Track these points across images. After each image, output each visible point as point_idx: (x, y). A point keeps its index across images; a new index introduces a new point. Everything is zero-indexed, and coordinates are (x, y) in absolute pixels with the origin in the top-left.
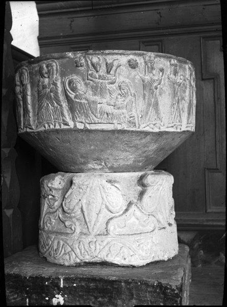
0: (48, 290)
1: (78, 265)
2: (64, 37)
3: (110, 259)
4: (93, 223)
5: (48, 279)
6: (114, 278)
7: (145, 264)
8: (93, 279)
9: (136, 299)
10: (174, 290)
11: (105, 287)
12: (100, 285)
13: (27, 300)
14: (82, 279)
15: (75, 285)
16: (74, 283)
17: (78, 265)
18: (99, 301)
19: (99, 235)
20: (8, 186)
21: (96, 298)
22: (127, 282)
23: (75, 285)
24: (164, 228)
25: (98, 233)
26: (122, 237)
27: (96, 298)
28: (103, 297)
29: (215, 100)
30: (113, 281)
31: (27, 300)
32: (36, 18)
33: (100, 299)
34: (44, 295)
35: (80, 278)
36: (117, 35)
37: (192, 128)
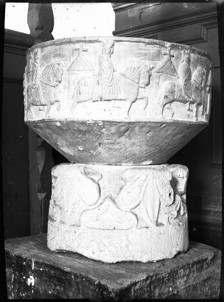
0: (25, 270)
1: (60, 252)
2: (133, 29)
3: (80, 251)
4: (69, 212)
5: (25, 260)
6: (67, 269)
7: (115, 262)
8: (52, 267)
9: (82, 295)
10: (110, 293)
11: (61, 277)
12: (58, 274)
13: (13, 275)
14: (46, 265)
15: (41, 269)
16: (41, 268)
17: (61, 252)
18: (57, 290)
19: (73, 225)
20: (40, 171)
21: (56, 285)
22: (75, 275)
23: (41, 269)
24: (147, 228)
25: (73, 223)
26: (93, 230)
27: (56, 285)
28: (60, 286)
29: (11, 35)
30: (67, 272)
31: (13, 275)
32: (113, 15)
33: (58, 288)
34: (23, 274)
35: (45, 264)
36: (179, 21)
37: (203, 119)
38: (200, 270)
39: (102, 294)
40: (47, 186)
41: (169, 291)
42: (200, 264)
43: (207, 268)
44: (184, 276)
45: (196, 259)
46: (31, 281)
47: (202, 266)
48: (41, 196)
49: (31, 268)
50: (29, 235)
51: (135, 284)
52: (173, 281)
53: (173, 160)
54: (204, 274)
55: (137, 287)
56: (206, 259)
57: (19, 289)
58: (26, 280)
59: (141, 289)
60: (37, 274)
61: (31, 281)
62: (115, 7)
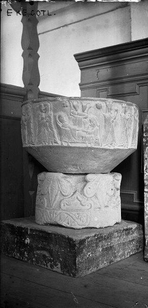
17: (46, 224)
20: (31, 177)
38: (127, 234)
39: (70, 243)
40: (34, 186)
41: (108, 244)
42: (128, 231)
43: (132, 234)
44: (118, 236)
45: (125, 228)
46: (28, 241)
47: (129, 233)
48: (31, 193)
49: (27, 233)
50: (19, 119)
51: (88, 238)
52: (111, 239)
53: (115, 170)
54: (130, 237)
55: (89, 240)
56: (132, 228)
57: (20, 247)
58: (24, 241)
59: (92, 241)
60: (31, 236)
61: (28, 241)
62: (83, 85)
